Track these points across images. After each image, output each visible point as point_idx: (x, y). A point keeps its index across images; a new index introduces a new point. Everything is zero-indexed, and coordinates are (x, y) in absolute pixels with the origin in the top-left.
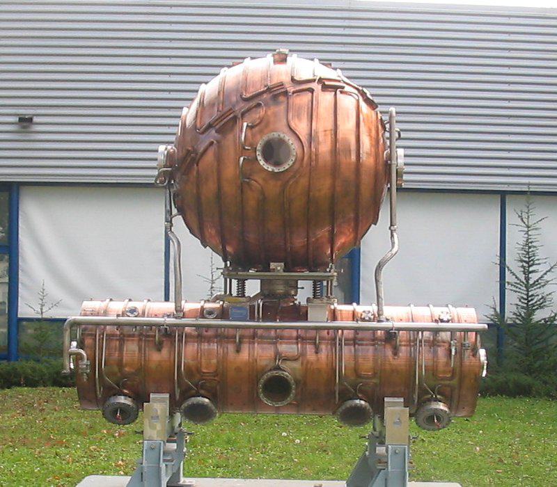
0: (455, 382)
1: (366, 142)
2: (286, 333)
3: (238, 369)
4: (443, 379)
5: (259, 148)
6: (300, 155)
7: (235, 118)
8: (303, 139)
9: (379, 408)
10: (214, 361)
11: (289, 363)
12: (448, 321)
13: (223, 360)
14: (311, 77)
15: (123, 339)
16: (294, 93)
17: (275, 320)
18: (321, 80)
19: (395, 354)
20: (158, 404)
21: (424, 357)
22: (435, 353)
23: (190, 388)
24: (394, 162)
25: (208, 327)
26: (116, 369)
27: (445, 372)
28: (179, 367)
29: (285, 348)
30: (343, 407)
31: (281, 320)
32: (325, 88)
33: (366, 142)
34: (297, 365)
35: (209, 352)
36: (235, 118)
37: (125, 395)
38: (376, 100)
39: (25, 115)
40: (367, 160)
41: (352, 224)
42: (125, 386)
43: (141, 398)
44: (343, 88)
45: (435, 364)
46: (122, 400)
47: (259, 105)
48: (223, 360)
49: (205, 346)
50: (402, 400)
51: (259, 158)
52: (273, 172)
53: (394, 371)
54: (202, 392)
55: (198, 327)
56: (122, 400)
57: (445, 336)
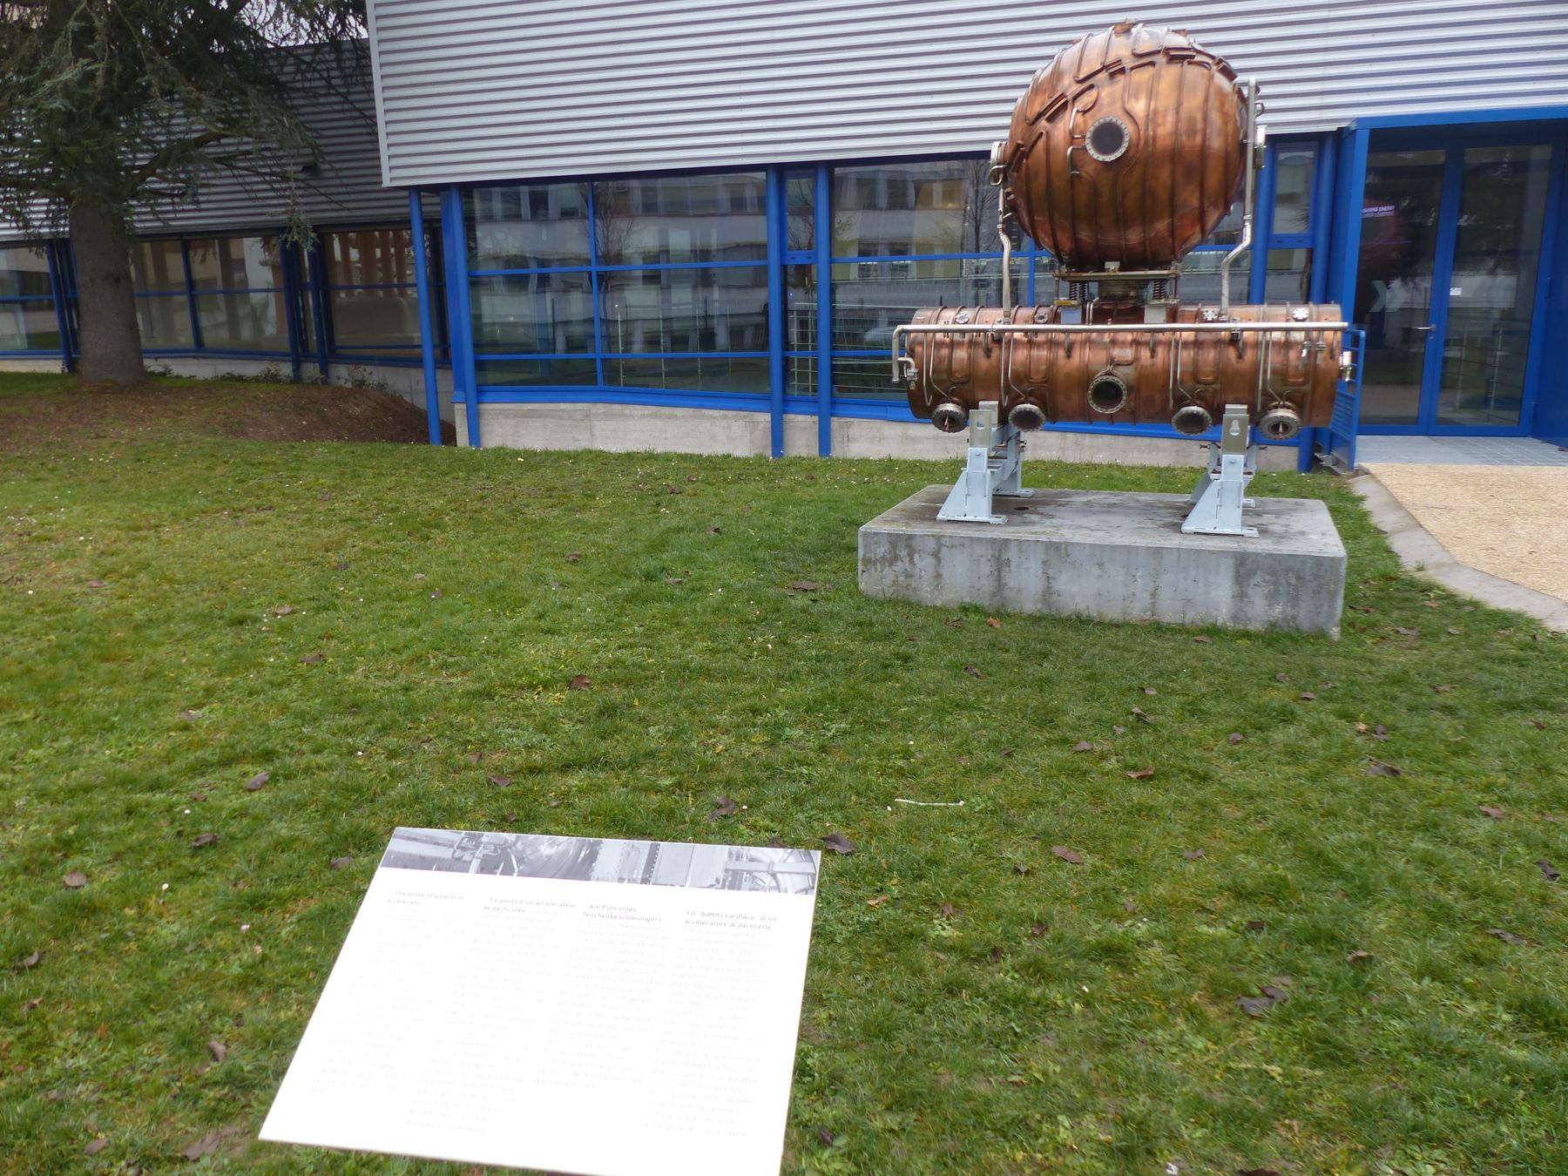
0: (1307, 388)
1: (1215, 117)
2: (1120, 337)
3: (1068, 375)
4: (1294, 384)
5: (1088, 135)
6: (1134, 137)
7: (1066, 104)
8: (1142, 127)
9: (1218, 413)
10: (1044, 367)
11: (1122, 369)
12: (1304, 320)
13: (1052, 365)
14: (1156, 49)
15: (953, 345)
16: (1132, 69)
17: (1106, 323)
18: (1167, 50)
19: (1240, 357)
20: (987, 412)
21: (1273, 359)
22: (1286, 355)
23: (1020, 396)
24: (1250, 141)
25: (1036, 332)
26: (945, 376)
27: (1296, 376)
28: (1006, 373)
29: (1117, 353)
30: (1178, 414)
31: (1114, 322)
32: (1172, 59)
33: (1215, 117)
34: (1129, 371)
35: (1039, 358)
36: (1066, 104)
37: (954, 402)
38: (1234, 64)
39: (425, 257)
40: (1216, 143)
41: (790, 242)
42: (953, 393)
43: (969, 404)
44: (1193, 57)
45: (484, 279)
46: (950, 407)
47: (1091, 87)
48: (1052, 365)
49: (1035, 353)
50: (1245, 407)
51: (1089, 147)
52: (1104, 163)
53: (1237, 373)
54: (1031, 399)
55: (1026, 332)
56: (950, 407)
57: (1298, 336)
